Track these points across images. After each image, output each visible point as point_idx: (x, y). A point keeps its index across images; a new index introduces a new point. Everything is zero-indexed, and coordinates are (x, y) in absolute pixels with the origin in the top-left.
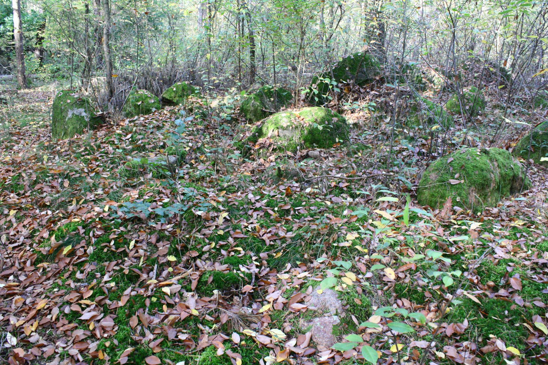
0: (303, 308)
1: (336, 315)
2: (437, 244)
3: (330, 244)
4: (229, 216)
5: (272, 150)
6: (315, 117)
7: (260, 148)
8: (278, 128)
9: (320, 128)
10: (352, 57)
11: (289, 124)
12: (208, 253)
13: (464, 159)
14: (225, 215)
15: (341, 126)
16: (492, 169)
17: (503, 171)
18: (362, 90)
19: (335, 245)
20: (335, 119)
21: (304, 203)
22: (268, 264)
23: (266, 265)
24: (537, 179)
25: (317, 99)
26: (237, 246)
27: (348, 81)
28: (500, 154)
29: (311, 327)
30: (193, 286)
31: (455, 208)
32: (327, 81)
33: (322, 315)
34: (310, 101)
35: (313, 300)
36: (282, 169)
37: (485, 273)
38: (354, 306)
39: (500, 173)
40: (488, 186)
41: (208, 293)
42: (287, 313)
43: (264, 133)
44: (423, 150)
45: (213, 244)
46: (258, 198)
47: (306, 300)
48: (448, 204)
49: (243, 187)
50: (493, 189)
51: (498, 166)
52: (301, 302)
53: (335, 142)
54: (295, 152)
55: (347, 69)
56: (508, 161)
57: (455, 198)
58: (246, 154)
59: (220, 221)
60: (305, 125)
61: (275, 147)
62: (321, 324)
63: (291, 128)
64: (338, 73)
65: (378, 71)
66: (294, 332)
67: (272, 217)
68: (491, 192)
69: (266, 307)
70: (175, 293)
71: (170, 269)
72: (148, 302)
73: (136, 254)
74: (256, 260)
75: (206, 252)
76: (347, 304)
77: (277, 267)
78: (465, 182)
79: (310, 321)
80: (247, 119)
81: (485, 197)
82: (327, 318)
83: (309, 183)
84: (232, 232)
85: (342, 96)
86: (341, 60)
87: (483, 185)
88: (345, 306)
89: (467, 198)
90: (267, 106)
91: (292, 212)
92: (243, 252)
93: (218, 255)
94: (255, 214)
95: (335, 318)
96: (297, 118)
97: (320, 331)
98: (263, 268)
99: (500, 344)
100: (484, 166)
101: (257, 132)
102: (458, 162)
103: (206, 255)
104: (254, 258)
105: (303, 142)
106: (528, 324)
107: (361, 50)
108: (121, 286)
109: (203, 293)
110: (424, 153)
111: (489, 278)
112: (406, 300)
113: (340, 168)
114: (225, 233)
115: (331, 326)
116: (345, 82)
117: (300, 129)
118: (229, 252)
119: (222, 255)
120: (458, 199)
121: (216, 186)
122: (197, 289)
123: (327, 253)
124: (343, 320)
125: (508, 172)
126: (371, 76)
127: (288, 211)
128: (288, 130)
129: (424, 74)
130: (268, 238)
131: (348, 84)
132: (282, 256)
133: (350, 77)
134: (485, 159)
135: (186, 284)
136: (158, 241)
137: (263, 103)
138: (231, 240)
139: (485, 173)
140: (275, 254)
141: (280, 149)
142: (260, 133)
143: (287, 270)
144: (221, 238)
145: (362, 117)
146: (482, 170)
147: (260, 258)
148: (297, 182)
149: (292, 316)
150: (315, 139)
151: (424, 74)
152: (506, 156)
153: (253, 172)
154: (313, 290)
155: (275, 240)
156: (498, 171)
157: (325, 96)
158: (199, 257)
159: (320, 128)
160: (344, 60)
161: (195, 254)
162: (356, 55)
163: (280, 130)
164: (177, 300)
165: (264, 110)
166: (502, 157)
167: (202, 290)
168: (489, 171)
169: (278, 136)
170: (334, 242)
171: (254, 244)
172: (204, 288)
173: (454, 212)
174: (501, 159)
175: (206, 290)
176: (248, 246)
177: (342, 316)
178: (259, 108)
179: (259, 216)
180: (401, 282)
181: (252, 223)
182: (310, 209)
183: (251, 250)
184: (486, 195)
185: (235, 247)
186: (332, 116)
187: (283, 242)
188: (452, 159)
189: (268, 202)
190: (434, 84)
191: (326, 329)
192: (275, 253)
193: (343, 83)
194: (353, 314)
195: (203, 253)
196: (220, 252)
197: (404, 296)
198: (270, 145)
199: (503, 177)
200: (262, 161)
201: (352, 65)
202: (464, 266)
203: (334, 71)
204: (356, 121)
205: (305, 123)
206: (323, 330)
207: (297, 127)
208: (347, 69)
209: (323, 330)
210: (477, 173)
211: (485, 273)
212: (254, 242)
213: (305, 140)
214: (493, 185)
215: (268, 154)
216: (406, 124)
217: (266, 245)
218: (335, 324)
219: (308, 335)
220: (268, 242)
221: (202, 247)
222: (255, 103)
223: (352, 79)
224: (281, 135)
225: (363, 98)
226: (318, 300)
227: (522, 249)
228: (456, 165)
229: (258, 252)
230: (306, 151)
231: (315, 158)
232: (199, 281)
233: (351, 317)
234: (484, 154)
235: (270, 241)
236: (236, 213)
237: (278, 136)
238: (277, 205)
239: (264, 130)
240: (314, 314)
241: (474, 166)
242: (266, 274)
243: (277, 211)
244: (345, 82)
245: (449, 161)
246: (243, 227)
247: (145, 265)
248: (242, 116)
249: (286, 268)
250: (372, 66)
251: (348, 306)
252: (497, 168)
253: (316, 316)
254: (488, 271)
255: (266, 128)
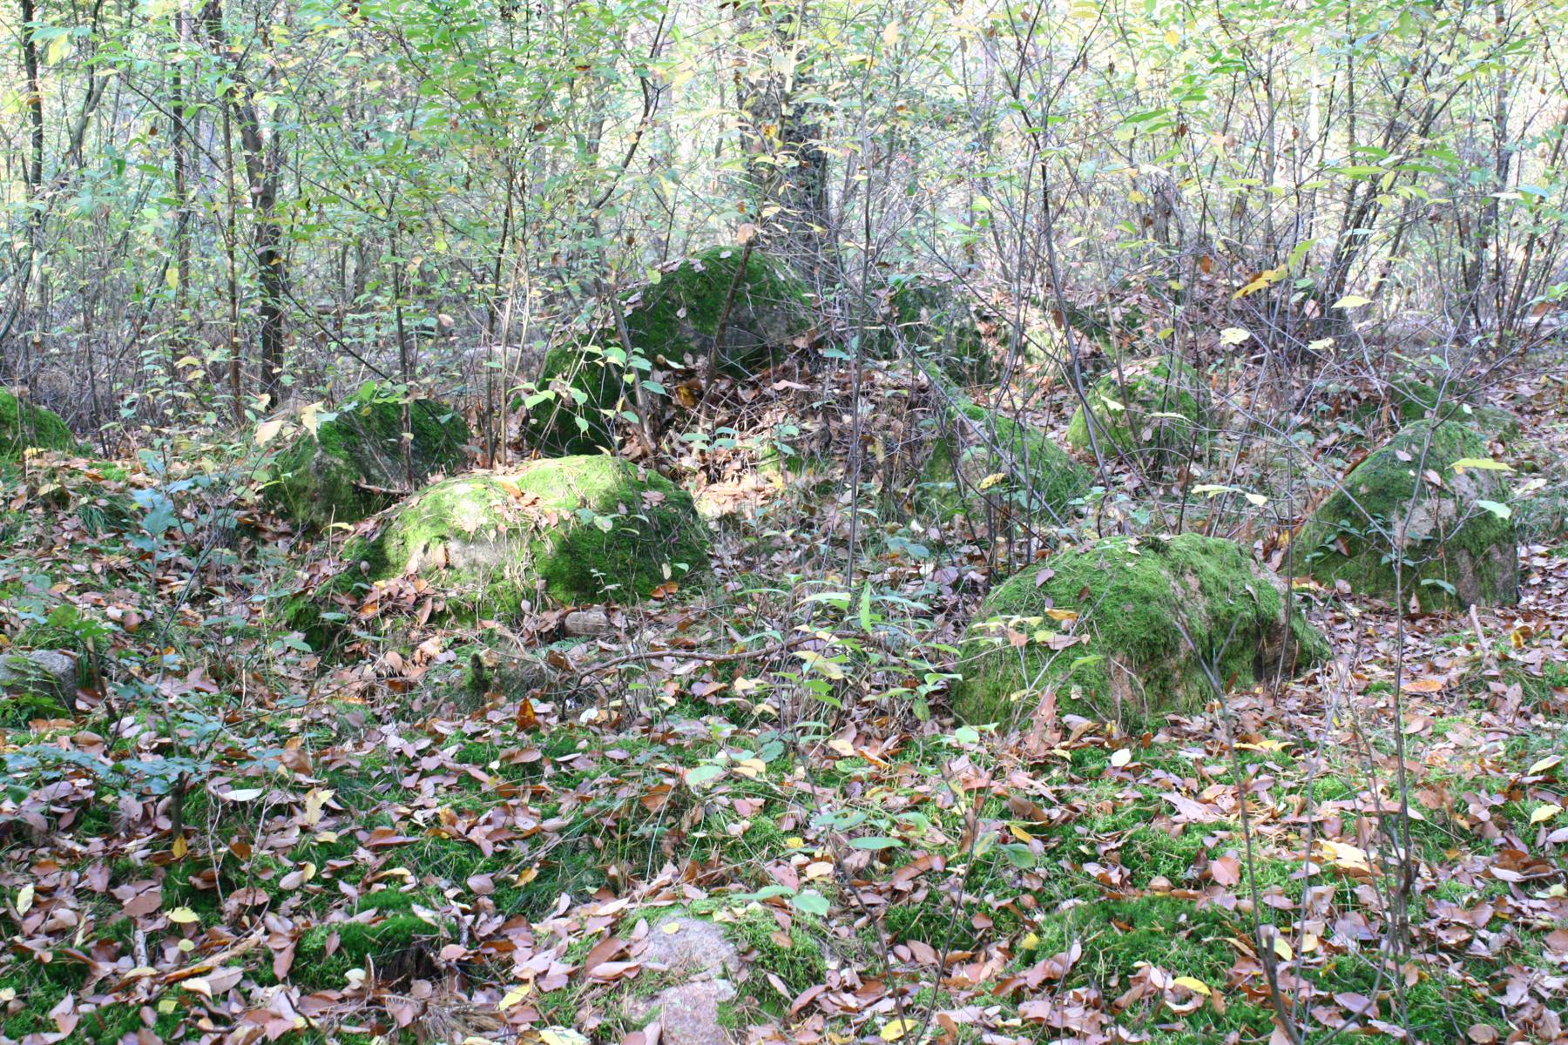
0: (628, 970)
1: (725, 977)
2: (1005, 804)
3: (685, 835)
4: (337, 801)
5: (429, 621)
6: (579, 491)
7: (383, 615)
8: (443, 538)
9: (605, 524)
10: (699, 267)
11: (484, 521)
12: (299, 895)
13: (1086, 569)
14: (326, 796)
15: (675, 520)
16: (1180, 597)
17: (1219, 605)
18: (746, 395)
19: (699, 835)
20: (654, 497)
21: (583, 744)
22: (498, 906)
23: (492, 910)
24: (1352, 636)
25: (583, 424)
26: (389, 865)
27: (688, 359)
28: (1205, 552)
29: (658, 1012)
30: (281, 966)
31: (1068, 718)
32: (616, 356)
33: (685, 979)
34: (555, 435)
35: (653, 949)
36: (487, 663)
37: (1142, 860)
38: (773, 953)
39: (1210, 611)
40: (1173, 650)
41: (329, 981)
42: (585, 986)
43: (393, 560)
44: (973, 575)
45: (311, 870)
46: (425, 743)
47: (632, 953)
48: (1046, 712)
49: (355, 729)
50: (1188, 659)
51: (1201, 588)
52: (622, 957)
53: (661, 580)
54: (515, 621)
55: (681, 313)
56: (1234, 574)
57: (1064, 688)
58: (330, 643)
59: (313, 815)
60: (543, 523)
61: (439, 607)
62: (684, 1002)
63: (493, 533)
64: (649, 326)
65: (802, 314)
66: (609, 1029)
67: (485, 788)
68: (1185, 670)
69: (514, 995)
70: (227, 993)
71: (186, 945)
72: (148, 1015)
73: (50, 923)
74: (456, 898)
75: (291, 892)
76: (753, 947)
77: (532, 907)
78: (1096, 641)
79: (653, 997)
80: (295, 527)
81: (1163, 688)
82: (699, 985)
83: (586, 697)
84: (362, 836)
85: (670, 422)
86: (655, 278)
87: (1151, 645)
88: (745, 954)
89: (1105, 689)
90: (374, 472)
91: (549, 770)
92: (411, 880)
93: (331, 898)
94: (427, 785)
95: (723, 984)
96: (511, 498)
97: (682, 1019)
98: (483, 917)
99: (1156, 976)
100: (1150, 588)
101: (365, 558)
102: (1067, 579)
103: (294, 901)
104: (450, 893)
105: (540, 584)
106: (1240, 940)
107: (729, 236)
108: (36, 998)
109: (313, 984)
110: (974, 583)
111: (1156, 869)
112: (920, 944)
113: (690, 647)
114: (340, 838)
115: (712, 1003)
116: (675, 365)
117: (526, 539)
118: (369, 886)
119: (344, 896)
120: (1075, 692)
121: (257, 732)
122: (294, 975)
123: (675, 863)
124: (745, 989)
125: (1238, 605)
126: (773, 338)
127: (534, 769)
128: (483, 542)
129: (986, 319)
130: (487, 837)
131: (690, 373)
132: (538, 880)
133: (693, 345)
134: (1153, 565)
135: (259, 970)
136: (114, 882)
137: (360, 464)
138: (363, 854)
139: (1154, 607)
140: (515, 877)
141: (464, 612)
142: (377, 560)
143: (562, 910)
144: (331, 850)
145: (753, 495)
146: (1147, 600)
147: (470, 892)
148: (544, 700)
149: (599, 991)
150: (588, 568)
151: (986, 319)
152: (1226, 557)
153: (368, 693)
154: (650, 927)
155: (510, 842)
156: (1203, 603)
157: (610, 413)
158: (274, 906)
159: (605, 524)
160: (669, 279)
161: (263, 897)
162: (712, 258)
163: (454, 546)
164: (236, 1008)
165: (363, 484)
166: (1215, 562)
167: (310, 972)
168: (1166, 601)
169: (447, 566)
170: (695, 828)
171: (447, 858)
172: (314, 969)
173: (1066, 731)
174: (1211, 567)
175: (322, 974)
176: (427, 864)
177: (740, 980)
178: (345, 479)
179: (441, 789)
180: (904, 901)
181: (422, 807)
182: (605, 758)
183: (439, 870)
184: (1165, 680)
185: (383, 868)
186: (642, 486)
187: (535, 845)
188: (1051, 574)
189: (460, 751)
190: (1029, 357)
191: (700, 1013)
192: (515, 872)
193: (668, 367)
194: (774, 971)
195: (282, 895)
196: (337, 889)
197: (916, 935)
198: (419, 601)
199: (1221, 623)
200: (392, 659)
201: (697, 298)
202: (1083, 848)
203: (631, 321)
204: (729, 507)
205: (543, 514)
206: (692, 1017)
207: (515, 531)
208: (681, 313)
209: (692, 1017)
210: (1130, 608)
211: (1142, 860)
212: (445, 851)
213: (549, 579)
214: (1186, 645)
215: (414, 634)
216: (919, 508)
217: (482, 855)
218: (721, 999)
219: (651, 1032)
220: (488, 848)
221: (278, 878)
222: (327, 460)
223: (703, 349)
224: (459, 561)
225: (753, 423)
226: (669, 946)
227: (1262, 805)
228: (1063, 590)
229: (460, 875)
230: (557, 614)
231: (592, 634)
232: (298, 953)
233: (765, 978)
234: (1151, 552)
235: (495, 844)
236: (362, 789)
237: (447, 566)
238: (494, 757)
239: (391, 549)
240: (664, 981)
241: (1117, 589)
242: (497, 931)
243: (500, 771)
244: (675, 365)
245: (1039, 582)
246: (395, 819)
247: (93, 944)
248: (277, 516)
249: (556, 908)
250: (778, 296)
251: (756, 954)
252: (1199, 596)
253: (668, 984)
254: (1151, 853)
255: (396, 542)
